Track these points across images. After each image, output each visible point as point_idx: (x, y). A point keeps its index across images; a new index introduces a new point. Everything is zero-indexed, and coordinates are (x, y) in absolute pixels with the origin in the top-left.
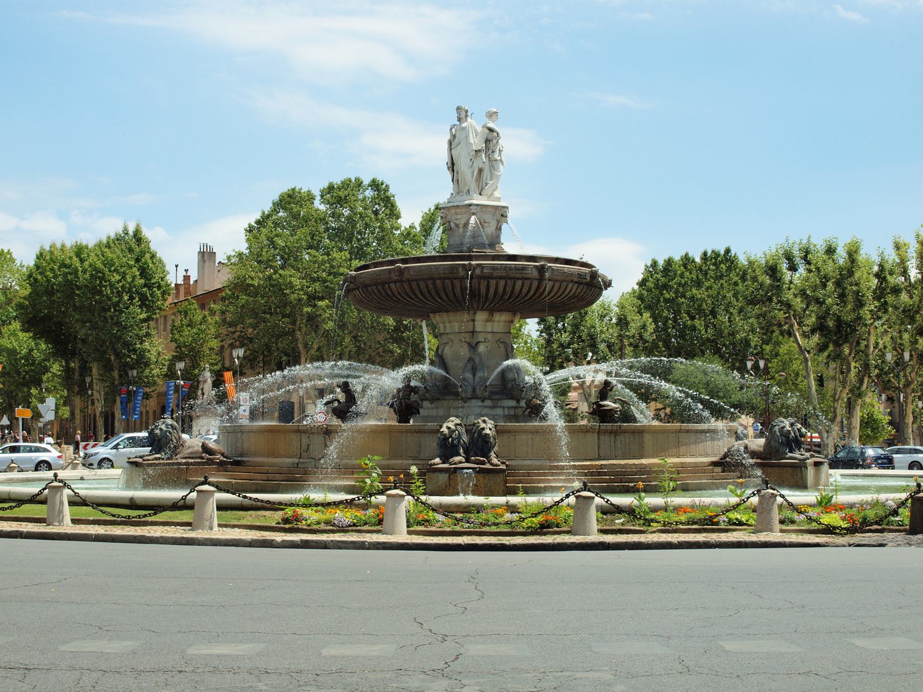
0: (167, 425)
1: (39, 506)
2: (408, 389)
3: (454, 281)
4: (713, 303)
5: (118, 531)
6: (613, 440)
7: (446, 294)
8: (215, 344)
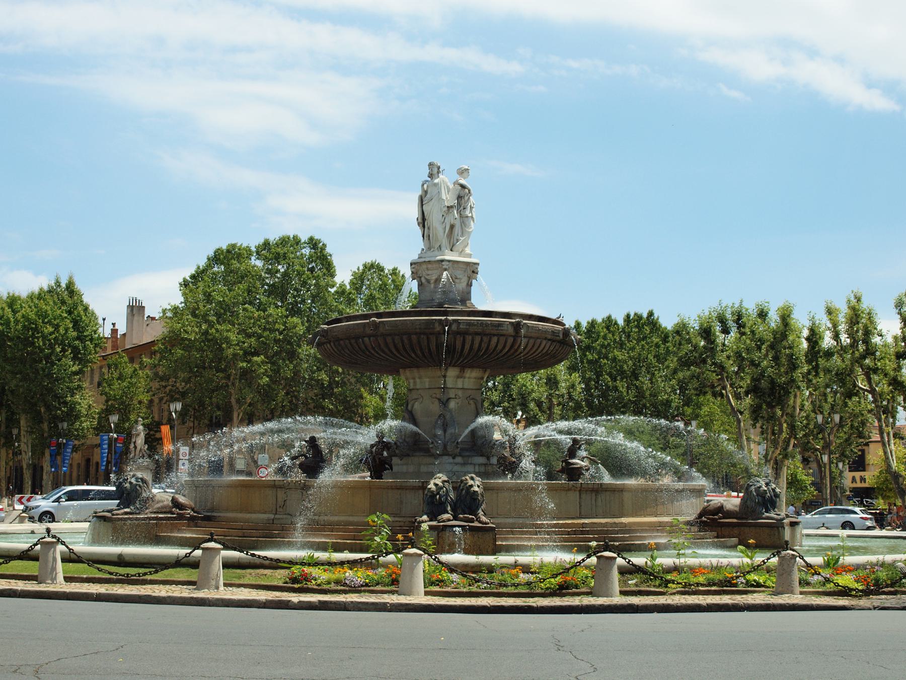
0: (137, 479)
1: (31, 563)
2: (381, 445)
3: (430, 336)
4: (634, 364)
5: (20, 585)
6: (594, 498)
7: (421, 349)
8: (145, 398)
